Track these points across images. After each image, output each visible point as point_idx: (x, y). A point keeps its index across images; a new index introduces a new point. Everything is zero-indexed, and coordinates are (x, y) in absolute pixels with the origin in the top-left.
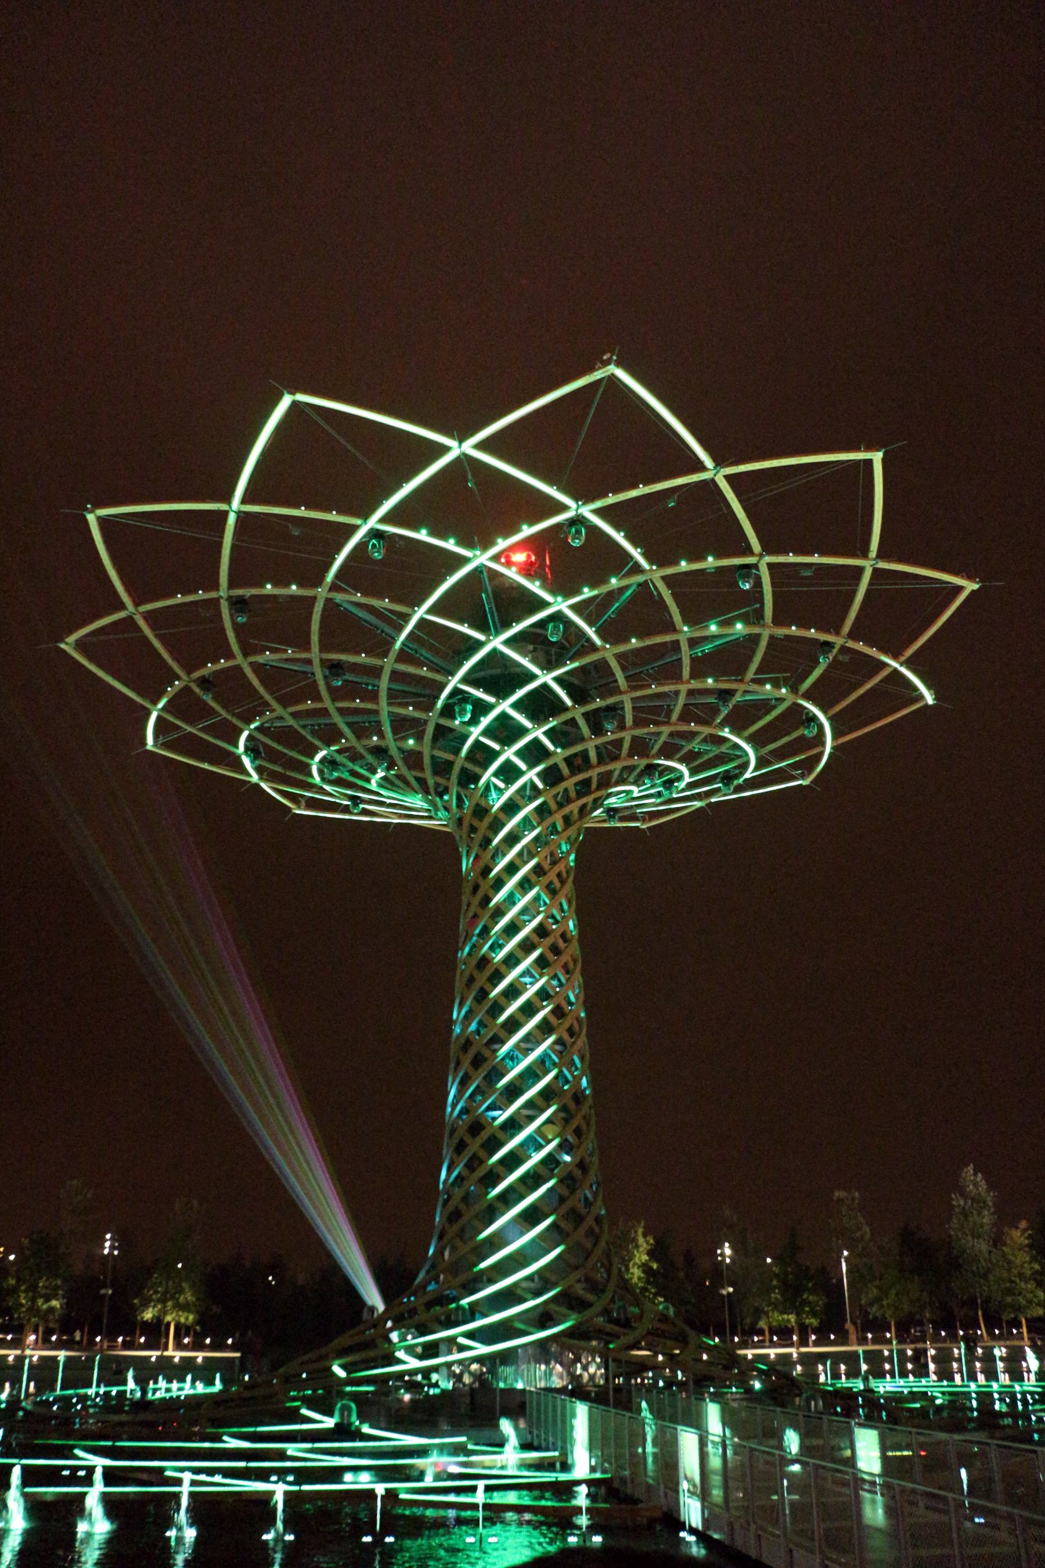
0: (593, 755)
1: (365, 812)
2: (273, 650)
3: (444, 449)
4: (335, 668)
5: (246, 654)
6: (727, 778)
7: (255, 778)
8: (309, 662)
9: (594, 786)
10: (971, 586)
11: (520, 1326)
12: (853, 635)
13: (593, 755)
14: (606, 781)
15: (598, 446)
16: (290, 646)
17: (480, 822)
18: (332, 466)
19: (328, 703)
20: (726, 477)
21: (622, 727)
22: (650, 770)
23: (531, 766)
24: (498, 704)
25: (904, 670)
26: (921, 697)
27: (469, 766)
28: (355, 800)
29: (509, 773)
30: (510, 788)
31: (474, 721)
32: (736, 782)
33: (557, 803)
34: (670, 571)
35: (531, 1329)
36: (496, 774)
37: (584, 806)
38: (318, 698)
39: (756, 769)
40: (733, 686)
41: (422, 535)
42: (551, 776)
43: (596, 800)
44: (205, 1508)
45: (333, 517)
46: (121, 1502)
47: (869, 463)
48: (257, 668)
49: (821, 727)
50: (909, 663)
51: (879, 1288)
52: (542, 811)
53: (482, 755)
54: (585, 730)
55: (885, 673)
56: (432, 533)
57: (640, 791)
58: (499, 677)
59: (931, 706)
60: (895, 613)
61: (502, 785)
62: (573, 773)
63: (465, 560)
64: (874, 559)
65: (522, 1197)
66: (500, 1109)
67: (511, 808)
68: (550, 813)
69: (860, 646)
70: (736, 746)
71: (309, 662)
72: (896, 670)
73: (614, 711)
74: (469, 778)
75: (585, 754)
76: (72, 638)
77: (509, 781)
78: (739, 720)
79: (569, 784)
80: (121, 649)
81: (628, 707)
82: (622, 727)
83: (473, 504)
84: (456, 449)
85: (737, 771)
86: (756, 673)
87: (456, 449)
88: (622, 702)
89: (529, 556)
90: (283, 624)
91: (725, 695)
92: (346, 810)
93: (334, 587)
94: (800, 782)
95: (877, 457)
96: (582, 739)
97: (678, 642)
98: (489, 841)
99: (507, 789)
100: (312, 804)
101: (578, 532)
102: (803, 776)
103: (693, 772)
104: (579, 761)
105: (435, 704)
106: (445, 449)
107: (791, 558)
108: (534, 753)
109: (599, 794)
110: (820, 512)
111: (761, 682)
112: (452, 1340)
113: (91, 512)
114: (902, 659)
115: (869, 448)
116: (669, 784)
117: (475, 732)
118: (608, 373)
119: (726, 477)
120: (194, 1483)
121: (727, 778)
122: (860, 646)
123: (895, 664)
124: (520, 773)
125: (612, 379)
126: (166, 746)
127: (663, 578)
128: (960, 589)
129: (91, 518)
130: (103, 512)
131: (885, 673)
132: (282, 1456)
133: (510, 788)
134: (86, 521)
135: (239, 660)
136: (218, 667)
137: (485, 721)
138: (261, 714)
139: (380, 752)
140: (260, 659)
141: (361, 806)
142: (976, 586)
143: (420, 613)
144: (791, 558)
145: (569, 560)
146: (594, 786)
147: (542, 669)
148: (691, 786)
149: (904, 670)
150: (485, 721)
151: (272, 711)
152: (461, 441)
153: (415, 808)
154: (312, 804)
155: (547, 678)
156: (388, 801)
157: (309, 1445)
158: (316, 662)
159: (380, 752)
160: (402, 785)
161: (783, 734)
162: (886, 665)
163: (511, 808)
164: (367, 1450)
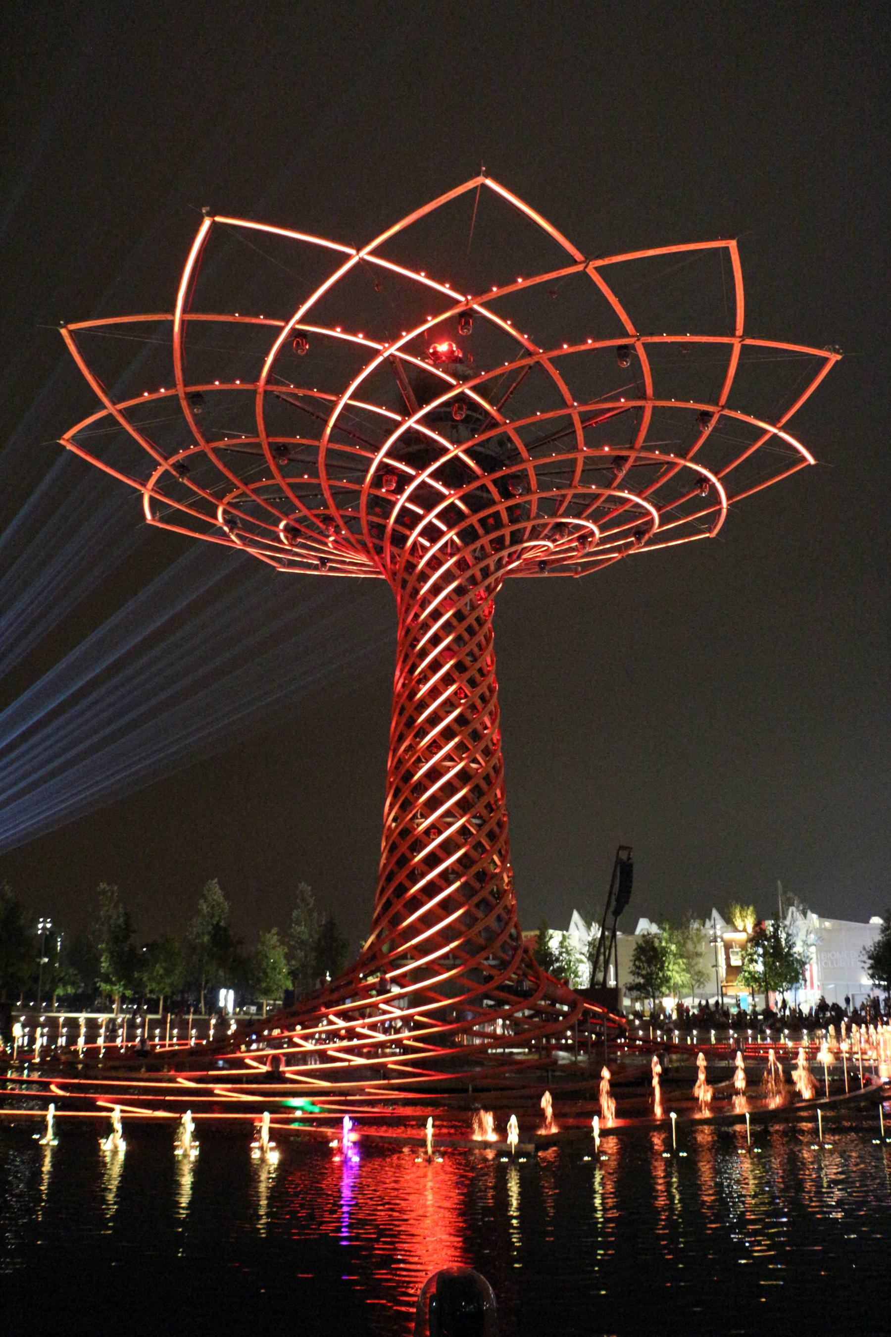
0: (505, 516)
1: (332, 569)
2: (230, 437)
3: (372, 253)
4: (280, 451)
5: (208, 441)
6: (639, 533)
7: (238, 544)
8: (258, 445)
9: (508, 542)
10: (835, 358)
11: (433, 995)
12: (731, 405)
13: (505, 516)
14: (517, 538)
15: (476, 246)
16: (244, 432)
17: (408, 576)
18: (254, 277)
19: (279, 480)
20: (596, 268)
21: (528, 491)
22: (560, 528)
23: (450, 528)
24: (418, 475)
25: (782, 434)
26: (804, 459)
27: (400, 528)
28: (323, 561)
29: (432, 533)
30: (434, 544)
31: (400, 490)
32: (647, 537)
33: (476, 558)
34: (555, 353)
35: (439, 997)
36: (421, 534)
37: (501, 559)
38: (271, 476)
39: (660, 526)
40: (624, 453)
41: (337, 333)
42: (468, 536)
43: (510, 555)
44: (131, 1128)
45: (261, 320)
46: (148, 1125)
47: (726, 250)
48: (215, 450)
49: (713, 487)
50: (784, 429)
51: (166, 969)
52: (462, 565)
53: (408, 519)
54: (496, 496)
55: (767, 437)
56: (344, 331)
57: (556, 546)
58: (417, 451)
59: (814, 466)
60: (767, 383)
61: (427, 544)
62: (487, 532)
63: (377, 352)
64: (740, 337)
65: (441, 890)
66: (454, 816)
67: (434, 563)
68: (469, 567)
69: (738, 415)
70: (638, 505)
71: (258, 445)
72: (775, 435)
73: (520, 478)
74: (399, 540)
75: (497, 515)
76: (67, 436)
77: (433, 541)
78: (637, 484)
79: (485, 540)
80: (104, 440)
81: (531, 473)
82: (528, 491)
83: (375, 303)
84: (356, 256)
85: (646, 527)
86: (645, 441)
87: (356, 256)
88: (526, 470)
89: (450, 345)
90: (234, 413)
91: (619, 461)
92: (316, 568)
93: (269, 381)
94: (707, 535)
95: (733, 244)
96: (493, 503)
97: (570, 415)
98: (417, 592)
99: (431, 547)
100: (292, 564)
101: (467, 323)
102: (710, 531)
103: (602, 529)
104: (491, 521)
105: (365, 477)
106: (348, 257)
107: (666, 338)
108: (451, 516)
109: (513, 549)
110: (664, 296)
111: (651, 449)
112: (375, 1005)
113: (64, 327)
114: (781, 425)
115: (724, 238)
116: (583, 539)
117: (402, 500)
118: (479, 183)
119: (596, 268)
120: (122, 1111)
121: (639, 533)
122: (738, 415)
123: (774, 430)
124: (442, 534)
125: (484, 186)
126: (161, 520)
127: (549, 359)
128: (826, 360)
129: (63, 331)
130: (72, 327)
131: (767, 437)
132: (210, 1093)
133: (434, 544)
134: (60, 334)
135: (202, 445)
136: (188, 453)
137: (409, 490)
138: (231, 491)
139: (328, 520)
140: (220, 444)
141: (329, 564)
142: (839, 357)
143: (345, 399)
144: (666, 338)
145: (479, 345)
146: (508, 542)
147: (453, 443)
148: (603, 541)
149: (782, 434)
150: (409, 490)
151: (238, 488)
152: (359, 250)
153: (356, 565)
154: (292, 564)
155: (455, 451)
156: (348, 560)
157: (229, 1086)
158: (265, 446)
159: (328, 520)
160: (347, 545)
161: (680, 494)
162: (765, 431)
163: (434, 563)
164: (300, 1090)
